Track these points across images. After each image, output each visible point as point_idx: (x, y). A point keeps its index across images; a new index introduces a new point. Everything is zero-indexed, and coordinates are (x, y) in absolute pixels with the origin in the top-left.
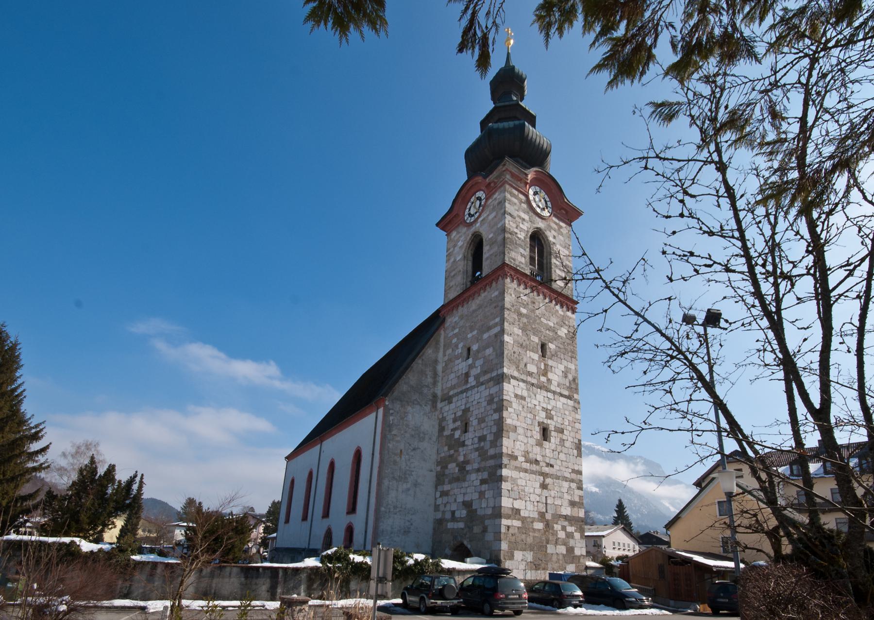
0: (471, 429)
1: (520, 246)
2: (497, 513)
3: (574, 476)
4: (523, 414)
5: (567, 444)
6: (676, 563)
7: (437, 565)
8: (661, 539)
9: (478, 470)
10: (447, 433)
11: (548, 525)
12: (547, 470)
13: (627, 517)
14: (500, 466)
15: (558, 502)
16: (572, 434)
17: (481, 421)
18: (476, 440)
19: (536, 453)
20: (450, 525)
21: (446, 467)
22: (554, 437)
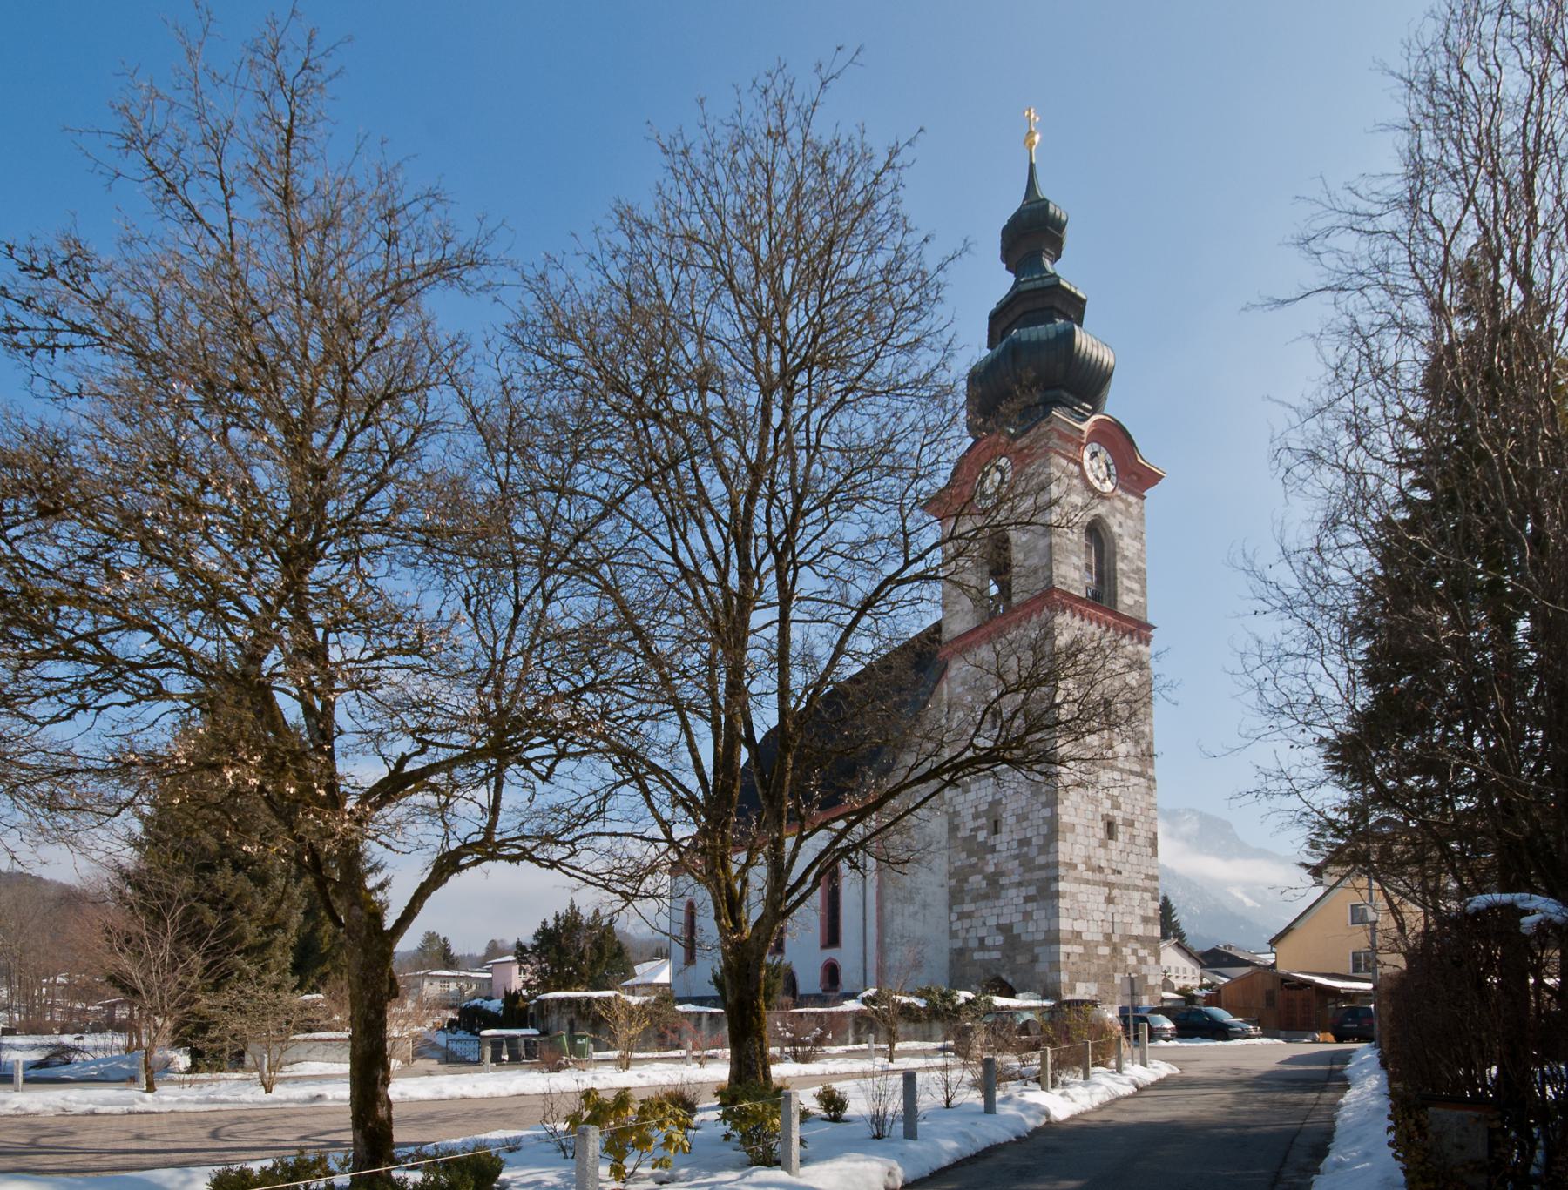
0: (1005, 829)
1: (1073, 552)
2: (1054, 938)
3: (1147, 883)
4: (1083, 807)
5: (1139, 841)
6: (1291, 987)
7: (990, 1002)
8: (1236, 958)
9: (1020, 884)
10: (962, 834)
11: (1115, 950)
12: (1113, 878)
13: (1177, 924)
14: (1056, 879)
15: (1127, 919)
16: (1146, 826)
17: (1021, 818)
18: (1015, 844)
19: (1100, 857)
20: (977, 956)
21: (966, 881)
22: (1122, 834)
